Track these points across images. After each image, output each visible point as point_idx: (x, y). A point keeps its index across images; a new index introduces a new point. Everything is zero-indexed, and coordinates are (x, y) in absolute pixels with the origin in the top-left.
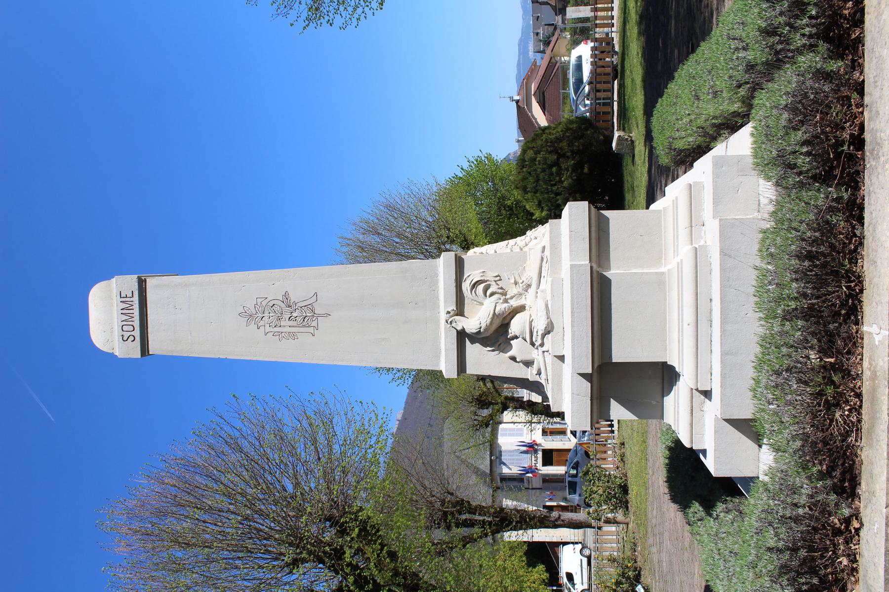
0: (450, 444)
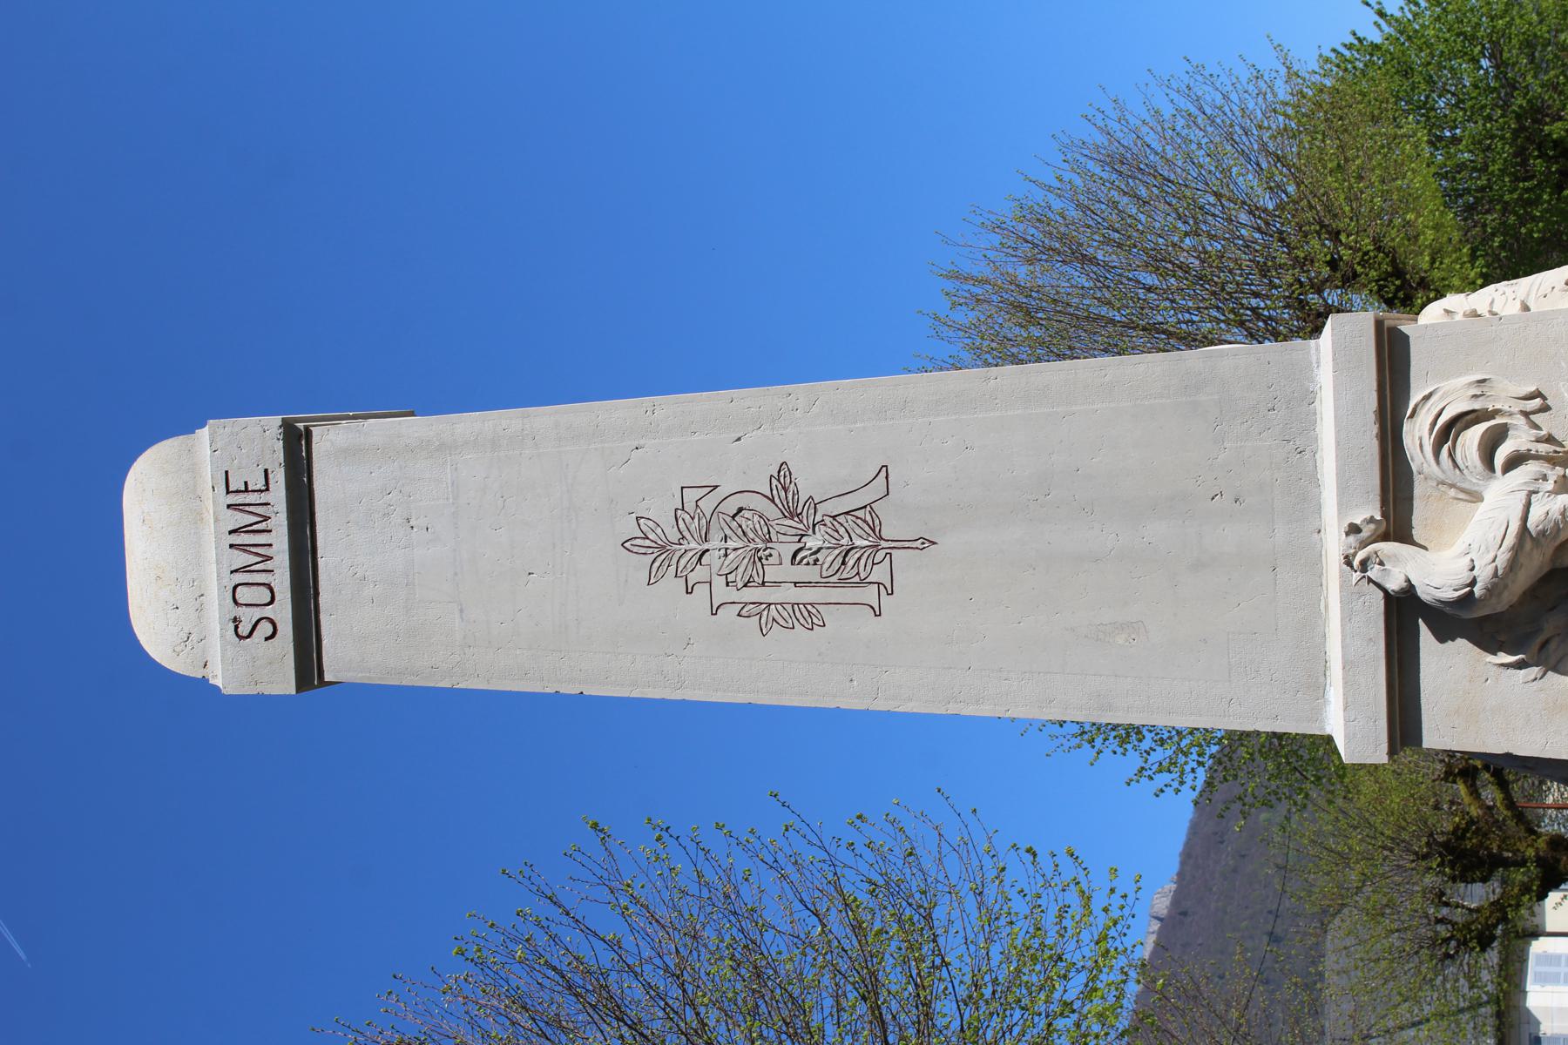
0: (1348, 1007)
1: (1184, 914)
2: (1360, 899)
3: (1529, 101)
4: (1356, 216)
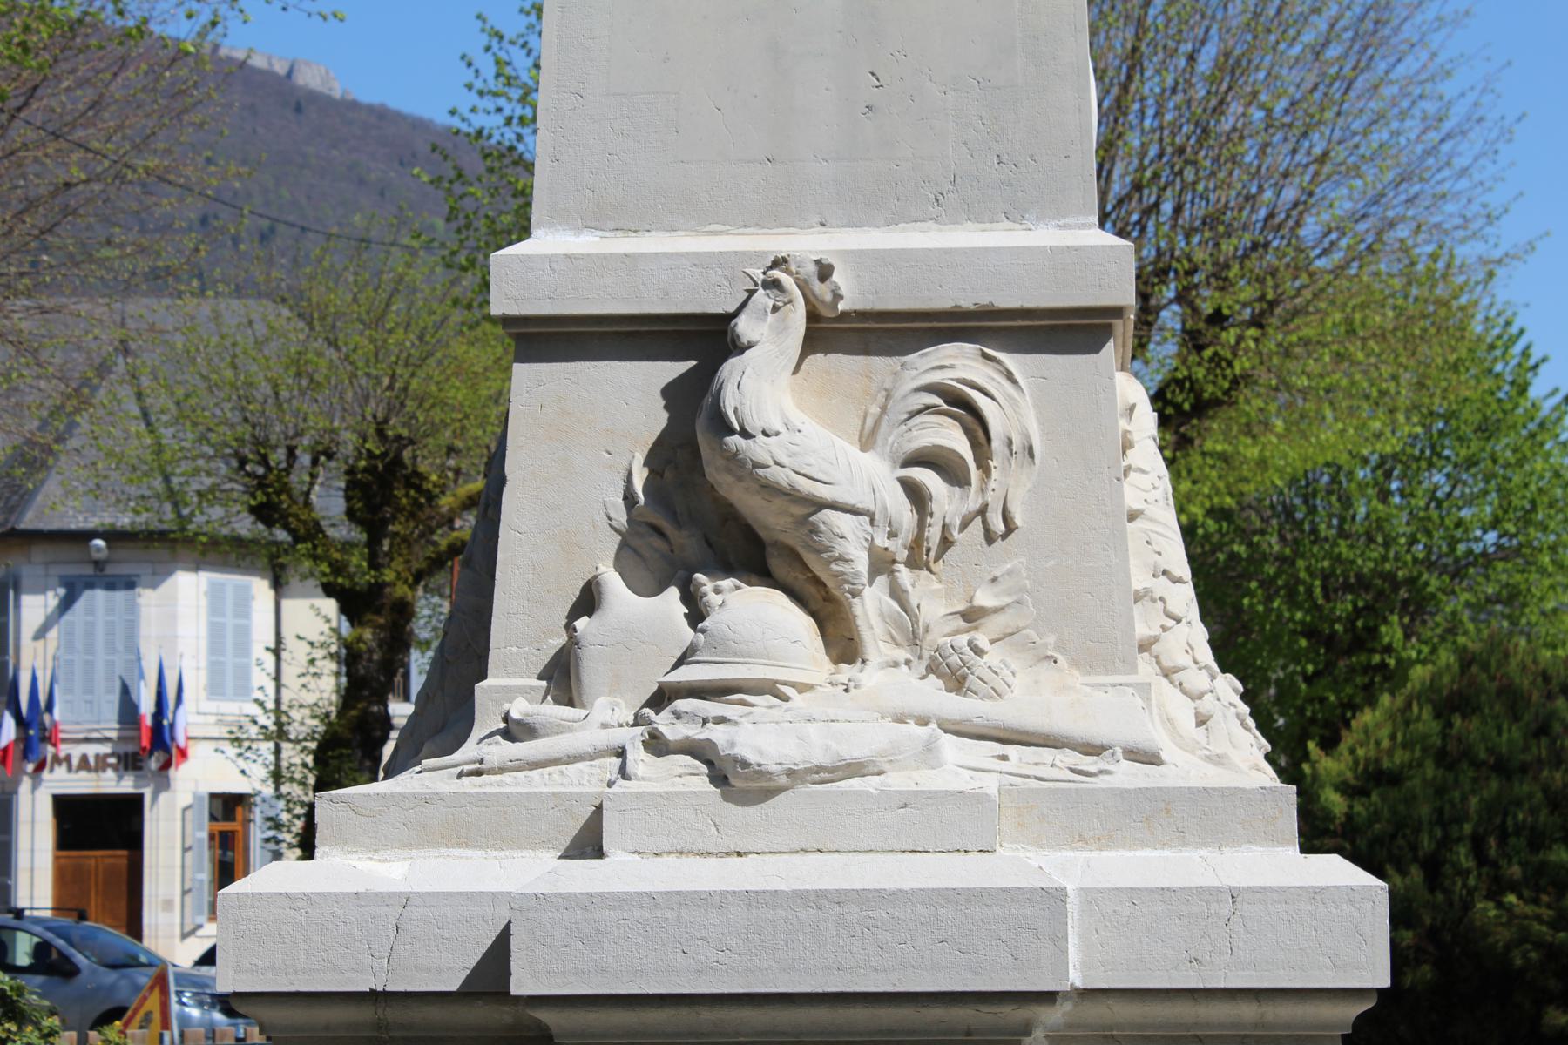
1: (298, 109)
2: (319, 344)
3: (1433, 596)
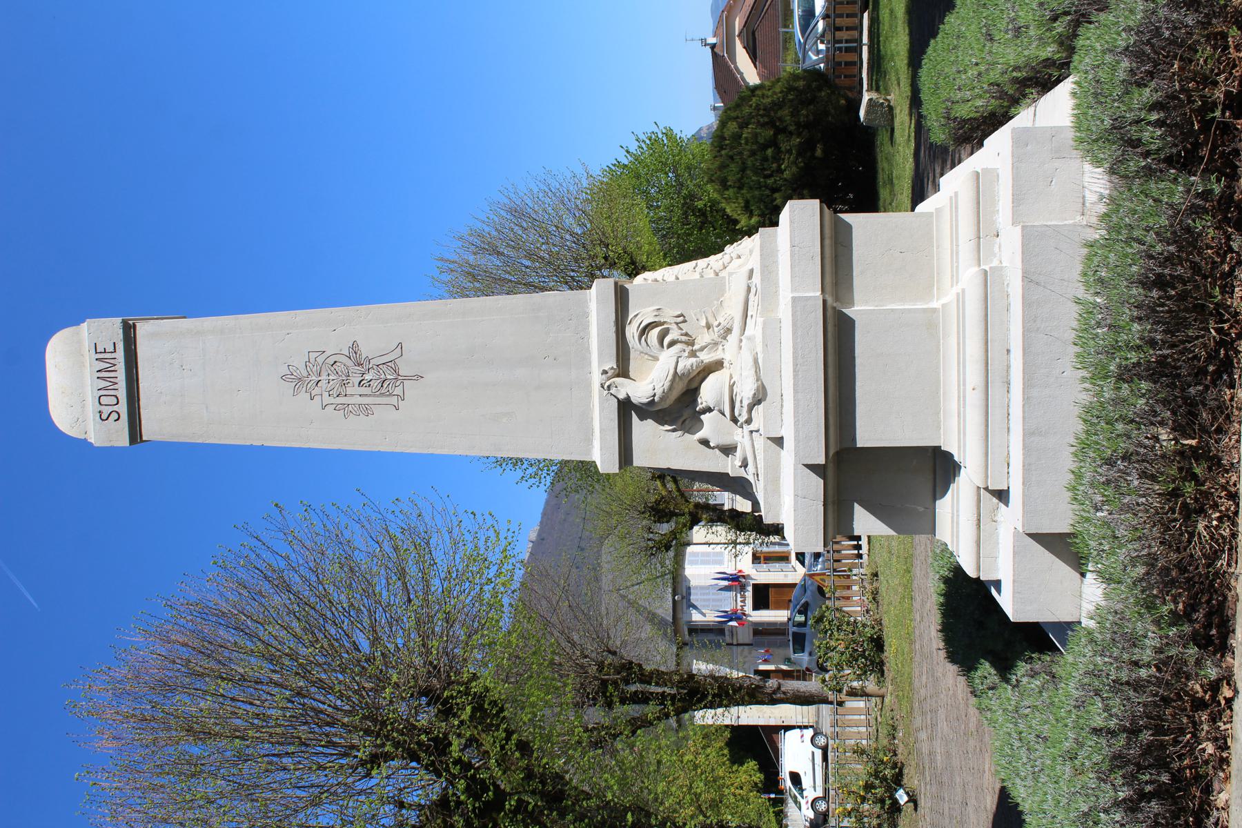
0: (610, 577)
4: (616, 237)
